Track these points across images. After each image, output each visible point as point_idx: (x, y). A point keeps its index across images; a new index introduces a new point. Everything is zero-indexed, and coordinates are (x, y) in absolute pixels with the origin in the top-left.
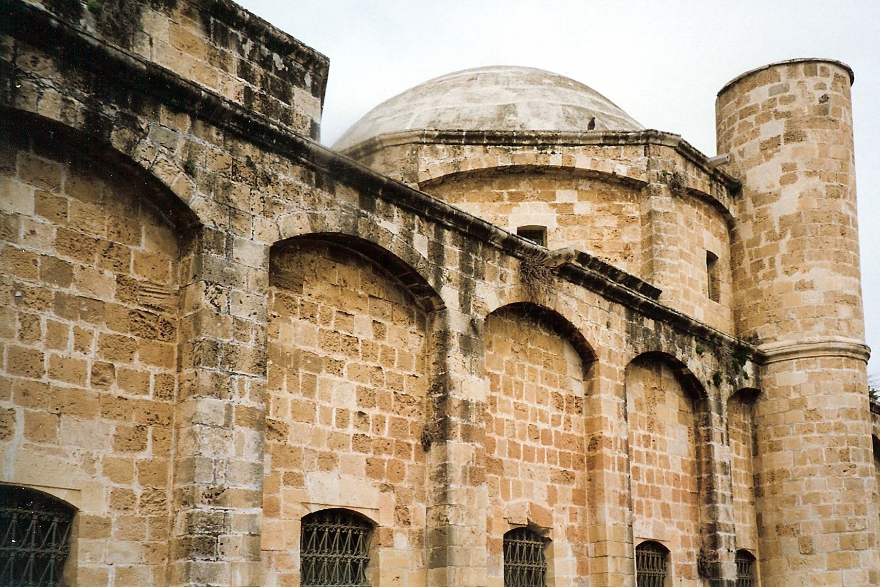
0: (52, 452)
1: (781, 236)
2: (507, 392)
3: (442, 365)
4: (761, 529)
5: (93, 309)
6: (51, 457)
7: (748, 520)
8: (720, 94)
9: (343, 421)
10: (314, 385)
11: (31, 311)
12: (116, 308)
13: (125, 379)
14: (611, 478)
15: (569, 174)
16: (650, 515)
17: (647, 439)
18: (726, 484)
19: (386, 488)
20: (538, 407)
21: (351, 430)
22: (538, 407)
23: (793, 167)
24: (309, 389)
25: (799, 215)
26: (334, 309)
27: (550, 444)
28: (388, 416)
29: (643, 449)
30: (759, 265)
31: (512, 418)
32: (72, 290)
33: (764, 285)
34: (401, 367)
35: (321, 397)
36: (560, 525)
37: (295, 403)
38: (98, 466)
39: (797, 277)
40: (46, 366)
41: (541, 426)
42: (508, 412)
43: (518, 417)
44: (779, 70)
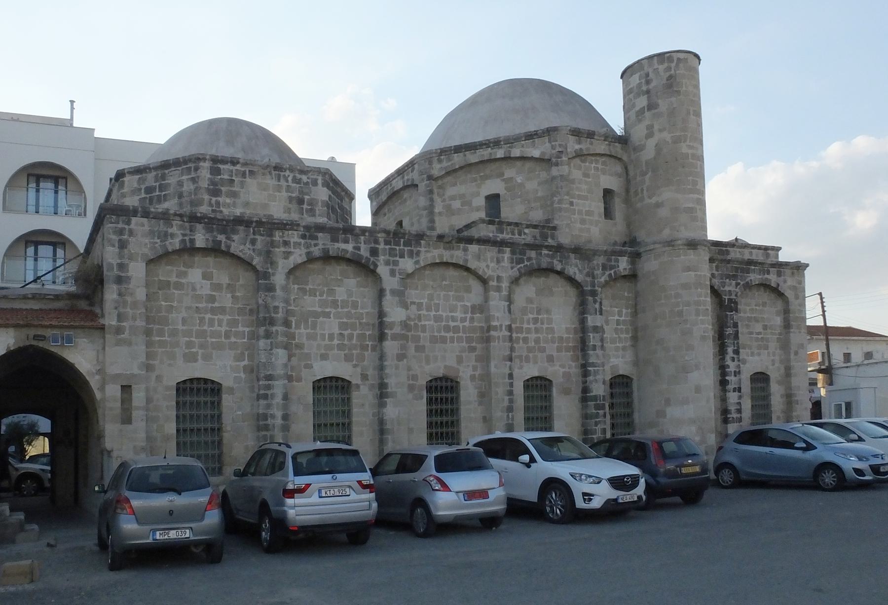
1: (646, 174)
2: (429, 309)
4: (636, 363)
5: (222, 310)
8: (622, 77)
11: (202, 315)
12: (231, 308)
13: (236, 334)
14: (499, 348)
17: (536, 321)
19: (355, 366)
21: (336, 342)
24: (314, 326)
26: (325, 289)
28: (355, 333)
29: (532, 326)
31: (432, 322)
32: (216, 305)
33: (639, 205)
34: (362, 308)
36: (466, 376)
41: (452, 324)
42: (429, 320)
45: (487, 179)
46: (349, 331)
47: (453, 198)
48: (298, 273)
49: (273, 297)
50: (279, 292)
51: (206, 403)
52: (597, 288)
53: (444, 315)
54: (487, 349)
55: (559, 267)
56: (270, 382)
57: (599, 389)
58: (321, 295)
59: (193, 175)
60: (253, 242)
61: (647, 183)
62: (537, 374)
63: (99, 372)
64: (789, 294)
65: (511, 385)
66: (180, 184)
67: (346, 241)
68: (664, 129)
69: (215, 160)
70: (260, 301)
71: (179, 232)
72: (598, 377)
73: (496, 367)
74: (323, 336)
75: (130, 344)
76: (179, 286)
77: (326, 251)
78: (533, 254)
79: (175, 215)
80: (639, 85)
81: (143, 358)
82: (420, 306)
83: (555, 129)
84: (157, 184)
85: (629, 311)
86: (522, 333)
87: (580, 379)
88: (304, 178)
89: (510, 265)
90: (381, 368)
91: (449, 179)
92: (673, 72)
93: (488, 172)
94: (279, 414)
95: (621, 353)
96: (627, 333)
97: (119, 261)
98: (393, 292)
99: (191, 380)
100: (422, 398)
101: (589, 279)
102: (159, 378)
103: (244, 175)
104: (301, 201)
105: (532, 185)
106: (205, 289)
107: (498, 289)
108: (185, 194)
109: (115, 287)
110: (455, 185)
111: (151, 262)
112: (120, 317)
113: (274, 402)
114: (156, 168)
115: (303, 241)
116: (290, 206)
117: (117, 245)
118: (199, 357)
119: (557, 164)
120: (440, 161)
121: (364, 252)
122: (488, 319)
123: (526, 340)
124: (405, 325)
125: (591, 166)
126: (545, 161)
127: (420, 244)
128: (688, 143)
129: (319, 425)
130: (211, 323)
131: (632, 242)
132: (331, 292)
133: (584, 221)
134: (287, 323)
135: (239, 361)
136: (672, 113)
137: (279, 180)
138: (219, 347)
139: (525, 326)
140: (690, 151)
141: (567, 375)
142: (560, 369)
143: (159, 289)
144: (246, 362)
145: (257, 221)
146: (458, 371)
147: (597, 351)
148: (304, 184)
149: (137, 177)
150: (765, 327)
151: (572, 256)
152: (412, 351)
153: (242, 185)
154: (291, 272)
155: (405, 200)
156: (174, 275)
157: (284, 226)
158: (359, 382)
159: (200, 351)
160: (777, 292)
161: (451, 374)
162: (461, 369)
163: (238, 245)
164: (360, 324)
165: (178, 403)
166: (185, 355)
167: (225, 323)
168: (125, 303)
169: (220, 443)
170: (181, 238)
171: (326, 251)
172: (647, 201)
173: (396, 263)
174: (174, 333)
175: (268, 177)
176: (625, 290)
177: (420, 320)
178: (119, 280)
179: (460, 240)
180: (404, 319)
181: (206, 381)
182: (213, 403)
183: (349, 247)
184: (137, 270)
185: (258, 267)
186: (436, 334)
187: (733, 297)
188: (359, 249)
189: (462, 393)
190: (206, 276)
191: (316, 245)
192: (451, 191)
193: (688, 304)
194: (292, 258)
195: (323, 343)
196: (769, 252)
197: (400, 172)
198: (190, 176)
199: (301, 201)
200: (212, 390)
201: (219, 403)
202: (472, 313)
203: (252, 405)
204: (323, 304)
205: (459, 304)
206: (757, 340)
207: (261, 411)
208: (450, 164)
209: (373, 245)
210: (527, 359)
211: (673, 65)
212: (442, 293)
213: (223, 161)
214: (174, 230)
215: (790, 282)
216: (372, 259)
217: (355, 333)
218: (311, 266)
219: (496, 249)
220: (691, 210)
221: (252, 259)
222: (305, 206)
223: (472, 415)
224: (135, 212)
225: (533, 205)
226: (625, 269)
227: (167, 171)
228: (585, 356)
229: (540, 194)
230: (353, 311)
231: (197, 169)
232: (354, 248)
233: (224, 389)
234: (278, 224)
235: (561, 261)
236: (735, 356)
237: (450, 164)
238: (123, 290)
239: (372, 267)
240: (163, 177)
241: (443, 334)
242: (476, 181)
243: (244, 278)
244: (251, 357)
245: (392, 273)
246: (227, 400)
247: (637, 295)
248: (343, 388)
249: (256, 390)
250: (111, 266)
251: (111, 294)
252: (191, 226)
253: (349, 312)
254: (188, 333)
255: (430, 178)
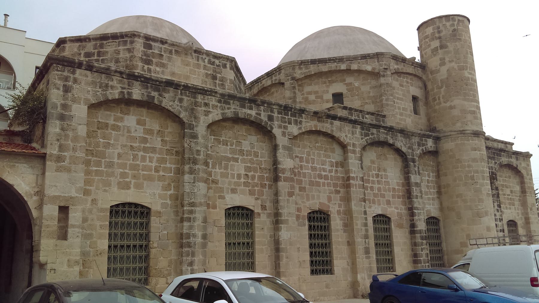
0: (142, 192)
1: (441, 87)
2: (307, 162)
3: (275, 156)
4: (441, 209)
5: (153, 150)
6: (142, 194)
7: (435, 204)
8: (418, 29)
9: (239, 177)
10: (228, 166)
11: (136, 153)
13: (165, 169)
14: (356, 192)
15: (348, 71)
16: (380, 204)
17: (377, 176)
18: (418, 191)
19: (257, 199)
20: (322, 167)
21: (242, 180)
22: (322, 167)
23: (444, 59)
24: (226, 168)
25: (447, 78)
26: (235, 141)
27: (328, 180)
28: (257, 175)
29: (375, 179)
30: (434, 99)
31: (310, 171)
32: (148, 145)
33: (437, 107)
34: (261, 157)
35: (231, 170)
37: (221, 173)
38: (157, 196)
39: (448, 104)
40: (141, 167)
42: (308, 170)
43: (312, 171)
44: (435, 20)
45: (333, 83)
46: (252, 173)
47: (310, 93)
48: (214, 128)
49: (197, 143)
50: (201, 140)
51: (135, 224)
52: (415, 157)
53: (318, 166)
54: (348, 193)
55: (391, 142)
56: (193, 208)
57: (421, 226)
58: (231, 145)
59: (128, 46)
60: (181, 100)
61: (443, 93)
62: (380, 213)
63: (37, 193)
64: (523, 172)
65: (366, 219)
66: (118, 52)
67: (251, 108)
68: (452, 61)
69: (148, 38)
70: (186, 145)
71: (119, 85)
72: (421, 217)
73: (355, 205)
74: (233, 175)
75: (69, 170)
76: (116, 128)
77: (236, 114)
78: (374, 131)
79: (116, 71)
80: (433, 34)
81: (81, 184)
82: (301, 159)
83: (382, 54)
84: (96, 51)
85: (434, 174)
86: (369, 183)
87: (408, 218)
88: (217, 62)
89: (360, 137)
90: (276, 202)
91: (307, 81)
92: (456, 27)
93: (334, 78)
94: (200, 234)
95: (431, 202)
96: (434, 189)
97: (63, 102)
98: (285, 147)
99: (124, 205)
100: (305, 225)
101: (410, 151)
102: (94, 201)
103: (171, 52)
104: (214, 78)
105: (365, 89)
106: (139, 132)
107: (354, 152)
108: (121, 60)
109: (58, 122)
110: (311, 85)
111: (93, 107)
112: (61, 148)
113: (196, 224)
114: (95, 39)
115: (219, 105)
116: (207, 80)
117: (61, 89)
118: (132, 186)
119: (384, 76)
120: (300, 68)
121: (264, 117)
122: (347, 172)
123: (372, 188)
124: (292, 170)
125: (404, 80)
126: (375, 75)
127: (302, 116)
128: (468, 71)
129: (230, 244)
130: (144, 159)
131: (433, 129)
132: (239, 143)
133: (401, 113)
134: (206, 164)
135: (166, 190)
136: (457, 51)
137: (198, 60)
138: (150, 178)
139: (371, 179)
140: (470, 76)
141: (400, 215)
142: (395, 210)
143: (98, 128)
144: (172, 192)
145: (184, 86)
146: (329, 207)
147: (419, 200)
148: (217, 66)
149: (77, 44)
150: (511, 192)
151: (399, 135)
152: (297, 191)
153: (170, 59)
154: (210, 126)
155: (273, 93)
156: (112, 118)
157: (204, 92)
158: (260, 211)
159: (133, 181)
160: (515, 170)
161: (325, 209)
162: (331, 205)
163: (168, 100)
164: (260, 168)
165: (110, 223)
166: (119, 183)
167: (155, 160)
168: (66, 136)
169: (147, 257)
170: (120, 90)
171: (236, 114)
172: (443, 104)
173: (285, 128)
174: (110, 165)
175: (189, 57)
176: (430, 161)
177: (302, 169)
178: (62, 118)
179: (329, 116)
180: (293, 167)
181: (136, 205)
182: (142, 224)
183: (253, 113)
184: (80, 111)
185: (185, 120)
186: (313, 180)
187: (494, 171)
188: (260, 115)
189: (332, 223)
190: (139, 122)
191: (228, 109)
192: (307, 89)
193: (477, 172)
194: (210, 116)
195: (233, 180)
196: (507, 145)
197: (269, 74)
198: (125, 47)
199: (214, 78)
200: (142, 213)
201: (148, 224)
202: (336, 167)
203: (176, 226)
204: (233, 152)
205: (327, 160)
206: (508, 199)
207: (185, 231)
208: (307, 71)
209: (270, 113)
210: (374, 202)
211: (456, 23)
212: (316, 152)
213: (155, 40)
214: (115, 83)
215: (523, 165)
216: (269, 123)
217: (257, 175)
218: (225, 124)
219: (351, 125)
220: (474, 112)
221: (180, 112)
222: (217, 82)
223: (340, 240)
224: (80, 65)
225: (367, 101)
226: (431, 147)
227: (105, 42)
228: (411, 202)
229: (371, 94)
230: (255, 159)
231: (132, 42)
232: (257, 114)
233: (152, 214)
234: (200, 89)
235: (392, 138)
236: (499, 209)
237: (307, 71)
238: (65, 126)
239: (269, 129)
240: (102, 46)
241: (317, 180)
242: (325, 83)
243: (171, 128)
244: (177, 188)
245: (284, 134)
246: (155, 222)
247: (438, 165)
248: (247, 215)
249: (181, 215)
250: (55, 106)
251: (53, 128)
252: (129, 82)
253: (252, 159)
254: (124, 166)
255: (293, 79)
